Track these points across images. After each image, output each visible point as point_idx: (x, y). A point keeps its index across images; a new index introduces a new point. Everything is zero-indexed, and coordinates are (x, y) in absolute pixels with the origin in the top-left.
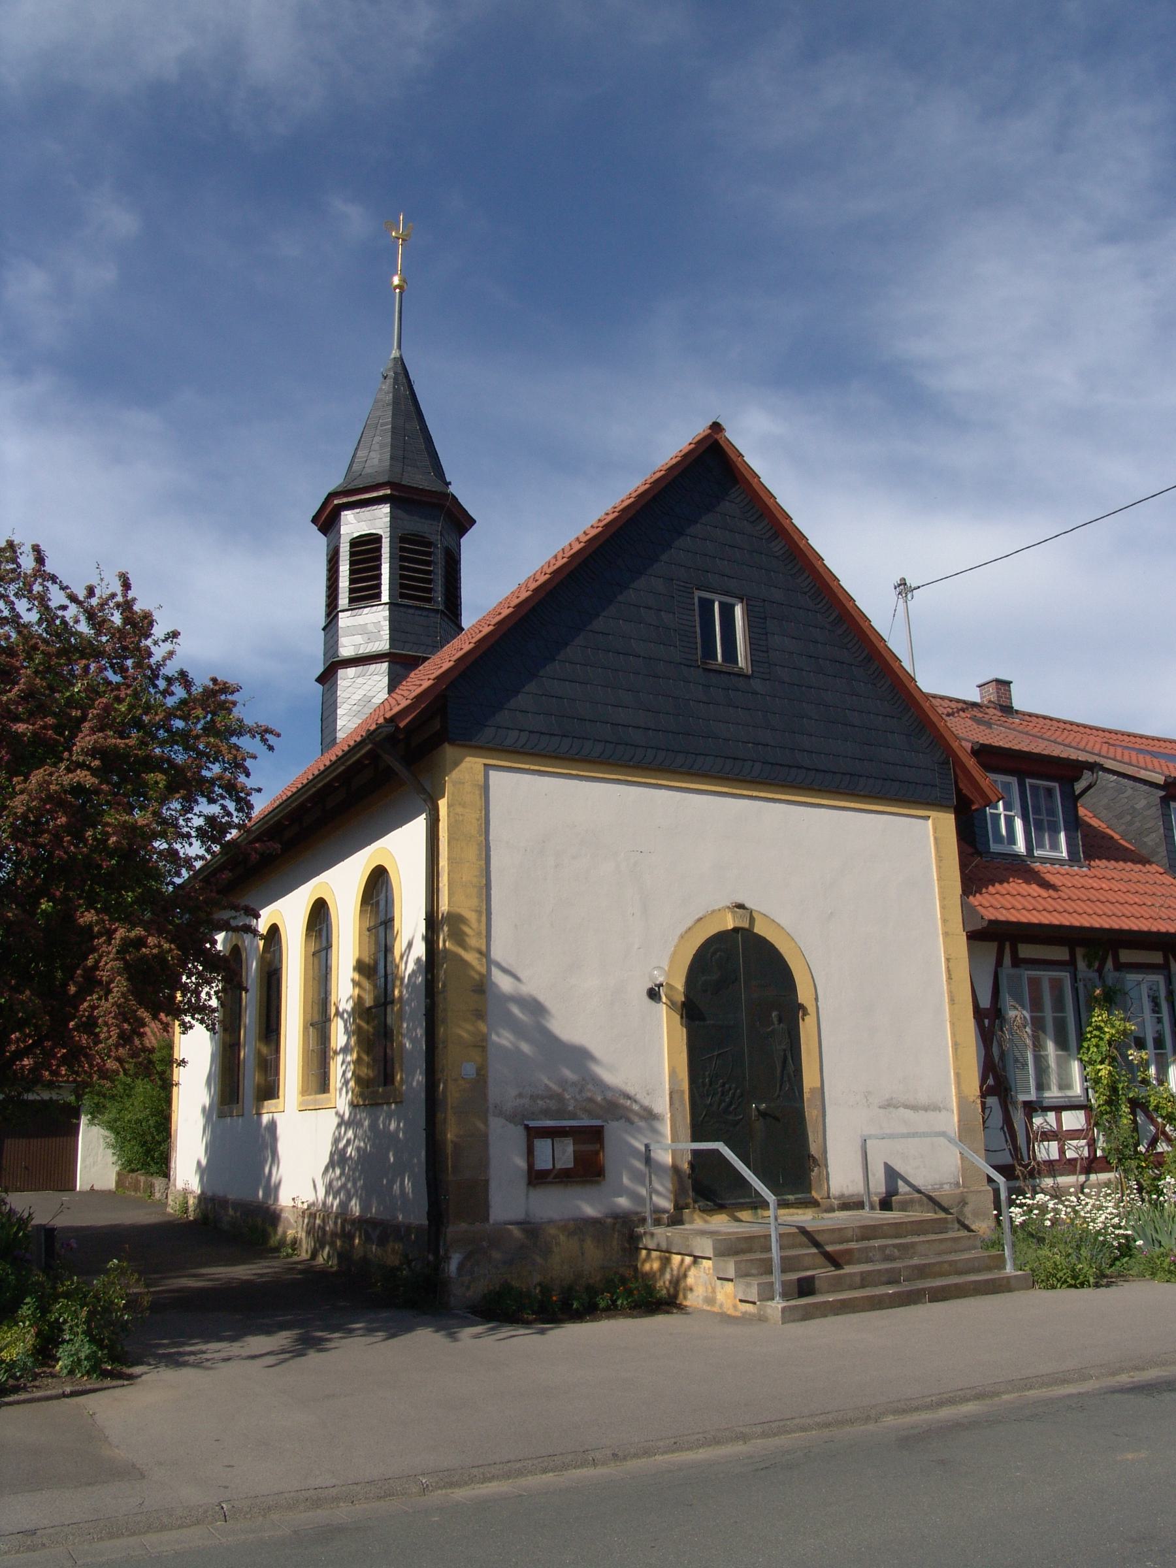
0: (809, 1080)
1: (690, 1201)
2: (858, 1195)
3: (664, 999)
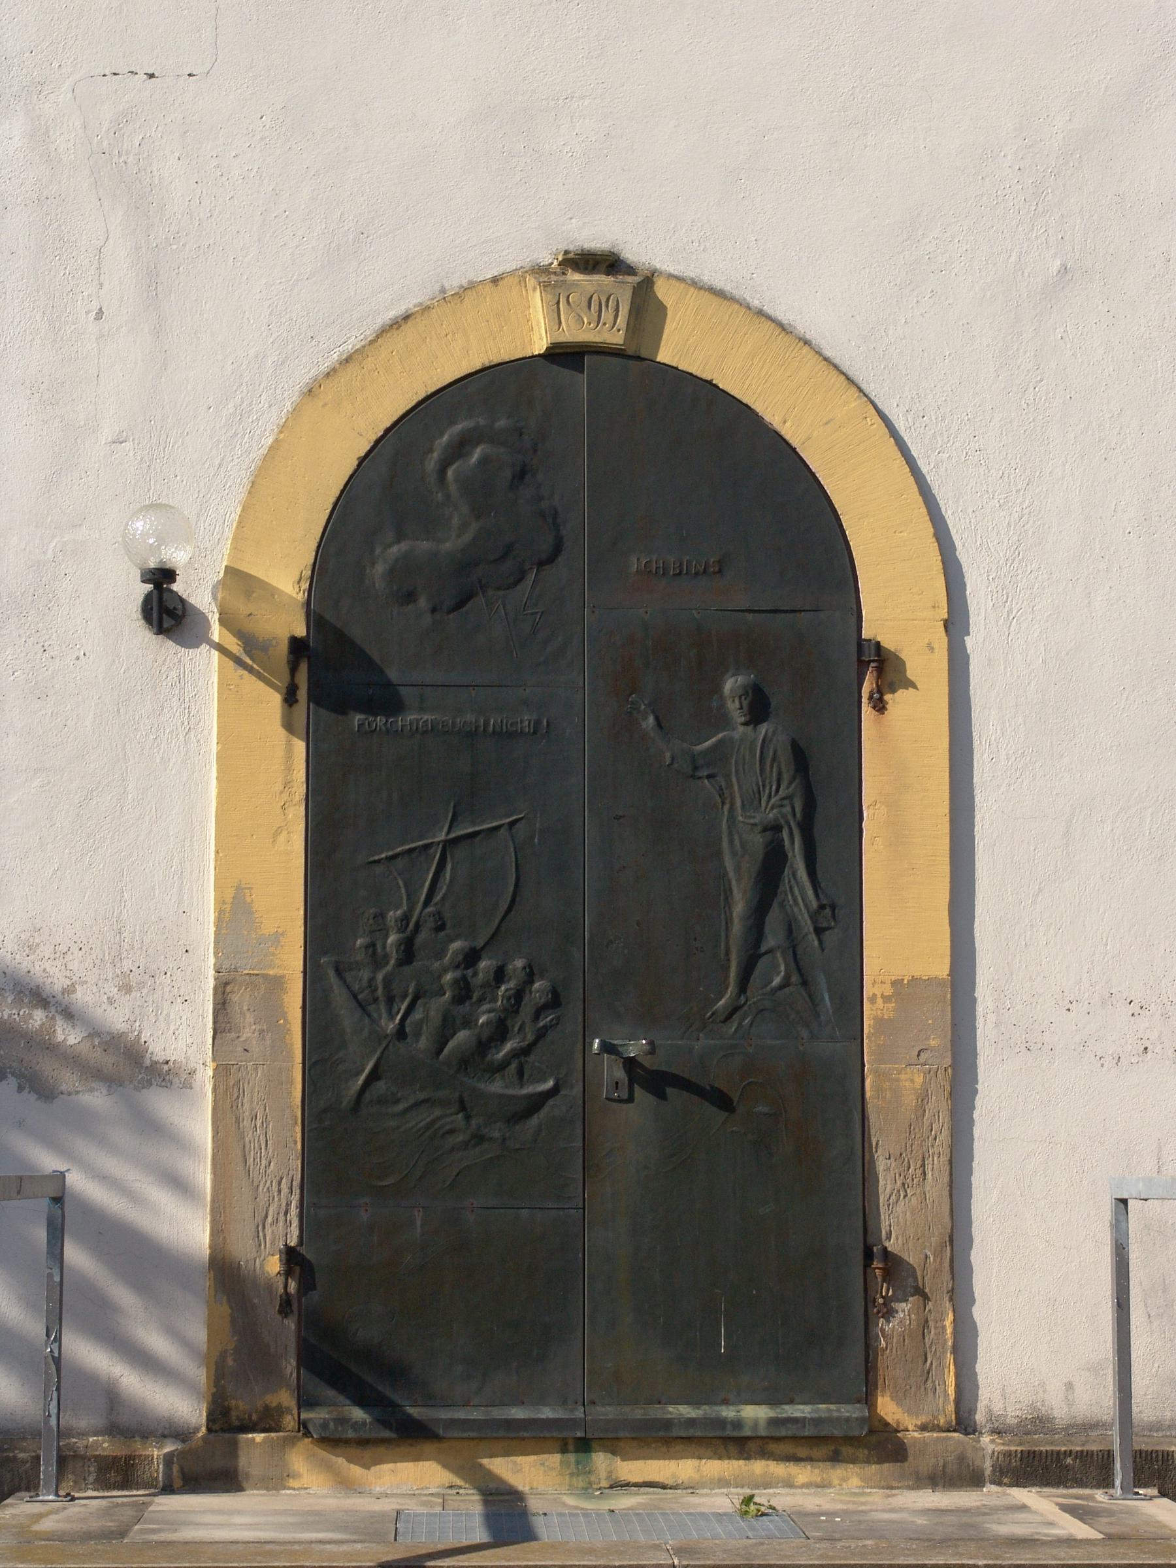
0: (896, 939)
1: (285, 1398)
2: (1089, 1426)
3: (216, 632)
